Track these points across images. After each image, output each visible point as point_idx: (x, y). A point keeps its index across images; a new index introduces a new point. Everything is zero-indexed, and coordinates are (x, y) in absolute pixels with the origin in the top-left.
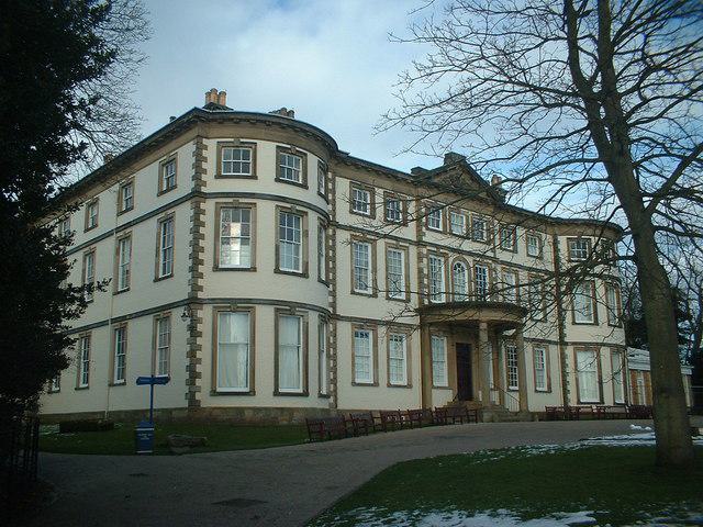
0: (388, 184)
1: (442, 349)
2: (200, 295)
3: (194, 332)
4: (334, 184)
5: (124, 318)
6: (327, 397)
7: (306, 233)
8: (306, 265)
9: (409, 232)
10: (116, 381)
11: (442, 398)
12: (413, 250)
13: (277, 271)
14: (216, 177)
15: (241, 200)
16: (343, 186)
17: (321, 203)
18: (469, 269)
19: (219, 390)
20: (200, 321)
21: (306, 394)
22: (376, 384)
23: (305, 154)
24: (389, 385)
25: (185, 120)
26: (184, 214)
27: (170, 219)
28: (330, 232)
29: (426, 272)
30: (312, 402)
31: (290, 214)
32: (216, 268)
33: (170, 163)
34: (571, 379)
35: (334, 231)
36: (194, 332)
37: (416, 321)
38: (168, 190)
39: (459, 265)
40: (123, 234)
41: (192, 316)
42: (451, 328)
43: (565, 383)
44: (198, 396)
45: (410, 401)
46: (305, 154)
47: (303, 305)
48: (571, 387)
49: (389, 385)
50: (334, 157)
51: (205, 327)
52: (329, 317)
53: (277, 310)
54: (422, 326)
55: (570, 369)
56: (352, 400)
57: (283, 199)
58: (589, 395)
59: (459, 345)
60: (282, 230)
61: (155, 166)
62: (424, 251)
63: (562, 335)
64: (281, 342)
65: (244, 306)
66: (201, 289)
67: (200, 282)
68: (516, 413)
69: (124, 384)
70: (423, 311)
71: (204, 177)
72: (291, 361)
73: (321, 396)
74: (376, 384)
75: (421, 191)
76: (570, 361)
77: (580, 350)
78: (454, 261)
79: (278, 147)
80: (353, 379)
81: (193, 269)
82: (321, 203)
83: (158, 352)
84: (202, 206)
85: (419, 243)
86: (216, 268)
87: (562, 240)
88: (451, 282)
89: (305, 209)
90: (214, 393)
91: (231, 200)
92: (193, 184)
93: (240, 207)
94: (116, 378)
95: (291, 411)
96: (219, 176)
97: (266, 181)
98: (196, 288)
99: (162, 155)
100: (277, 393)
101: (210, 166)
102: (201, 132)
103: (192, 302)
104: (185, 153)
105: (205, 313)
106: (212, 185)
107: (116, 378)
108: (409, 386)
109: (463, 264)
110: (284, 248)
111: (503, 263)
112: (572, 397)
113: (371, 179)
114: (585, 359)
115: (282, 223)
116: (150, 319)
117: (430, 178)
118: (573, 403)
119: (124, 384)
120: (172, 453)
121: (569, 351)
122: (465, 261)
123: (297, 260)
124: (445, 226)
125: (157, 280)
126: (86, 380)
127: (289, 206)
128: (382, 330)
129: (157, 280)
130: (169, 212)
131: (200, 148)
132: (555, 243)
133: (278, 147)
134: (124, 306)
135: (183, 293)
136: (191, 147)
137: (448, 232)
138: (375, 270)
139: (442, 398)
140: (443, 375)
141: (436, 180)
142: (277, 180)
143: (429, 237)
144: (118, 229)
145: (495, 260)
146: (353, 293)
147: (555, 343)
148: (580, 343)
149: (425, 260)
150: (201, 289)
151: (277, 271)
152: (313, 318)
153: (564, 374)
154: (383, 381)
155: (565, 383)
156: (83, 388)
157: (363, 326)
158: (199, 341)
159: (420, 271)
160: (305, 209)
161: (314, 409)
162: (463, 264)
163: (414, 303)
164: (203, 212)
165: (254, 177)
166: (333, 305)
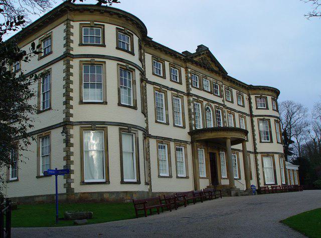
0: (171, 60)
1: (202, 155)
2: (71, 119)
3: (67, 142)
4: (144, 56)
7: (134, 82)
8: (135, 101)
9: (183, 88)
10: (11, 179)
11: (204, 184)
12: (185, 98)
13: (120, 104)
14: (79, 45)
15: (96, 59)
16: (148, 58)
17: (139, 64)
18: (213, 110)
19: (86, 181)
20: (71, 136)
21: (138, 182)
22: (170, 176)
23: (132, 35)
24: (177, 177)
26: (58, 70)
28: (144, 84)
29: (193, 111)
30: (142, 188)
31: (126, 69)
32: (81, 102)
34: (260, 172)
36: (67, 142)
37: (188, 139)
39: (208, 108)
41: (66, 133)
42: (207, 143)
43: (258, 175)
44: (73, 186)
45: (186, 186)
46: (105, 62)
47: (135, 127)
48: (261, 176)
49: (177, 177)
50: (147, 43)
51: (74, 140)
52: (147, 135)
53: (120, 129)
54: (192, 143)
55: (260, 167)
56: (161, 186)
58: (270, 181)
59: (211, 154)
60: (121, 79)
62: (191, 99)
63: (255, 148)
64: (124, 150)
65: (100, 127)
66: (72, 115)
67: (71, 111)
68: (245, 191)
69: (17, 180)
70: (192, 133)
71: (72, 45)
72: (128, 162)
74: (170, 176)
75: (189, 65)
76: (259, 162)
77: (264, 156)
78: (206, 105)
79: (117, 28)
80: (159, 174)
81: (66, 103)
82: (139, 64)
83: (41, 159)
84: (71, 63)
85: (189, 94)
86: (81, 102)
87: (253, 97)
88: (205, 120)
89: (134, 68)
90: (83, 183)
91: (89, 59)
92: (64, 49)
93: (94, 64)
94: (11, 176)
95: (131, 193)
96: (81, 45)
97: (110, 49)
98: (68, 115)
99: (42, 34)
100: (122, 182)
101: (75, 38)
102: (69, 17)
103: (66, 125)
104: (58, 32)
105: (75, 131)
106: (77, 50)
108: (187, 177)
109: (210, 108)
110: (122, 90)
111: (227, 108)
112: (261, 181)
113: (163, 56)
114: (267, 162)
115: (121, 75)
117: (192, 58)
118: (262, 185)
119: (17, 180)
120: (76, 224)
121: (259, 157)
122: (211, 106)
123: (130, 99)
124: (200, 85)
127: (125, 64)
128: (172, 144)
130: (47, 69)
131: (69, 27)
132: (250, 99)
135: (60, 118)
136: (63, 27)
137: (201, 89)
138: (167, 109)
139: (204, 184)
140: (203, 172)
141: (195, 59)
142: (118, 48)
143: (194, 91)
145: (224, 106)
146: (156, 122)
147: (252, 153)
148: (265, 153)
149: (192, 104)
150: (72, 115)
151: (120, 104)
152: (140, 134)
153: (257, 170)
154: (174, 175)
155: (258, 175)
157: (163, 141)
158: (72, 149)
159: (190, 110)
160: (134, 68)
161: (143, 192)
162: (210, 108)
163: (187, 129)
164: (72, 67)
165: (104, 46)
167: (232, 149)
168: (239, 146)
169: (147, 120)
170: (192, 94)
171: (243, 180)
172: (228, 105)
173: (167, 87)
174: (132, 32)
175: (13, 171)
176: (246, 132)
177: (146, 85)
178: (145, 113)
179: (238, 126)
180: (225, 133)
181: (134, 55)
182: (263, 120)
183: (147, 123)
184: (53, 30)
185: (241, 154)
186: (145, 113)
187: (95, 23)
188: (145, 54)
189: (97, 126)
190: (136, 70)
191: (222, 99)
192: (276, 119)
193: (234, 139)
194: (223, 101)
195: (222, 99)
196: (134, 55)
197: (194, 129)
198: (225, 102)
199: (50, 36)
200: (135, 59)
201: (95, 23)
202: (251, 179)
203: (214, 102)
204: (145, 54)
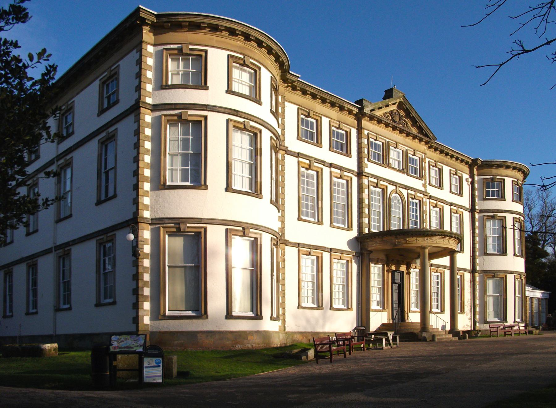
4: (283, 108)
5: (68, 244)
6: (277, 319)
13: (229, 188)
17: (271, 120)
23: (260, 69)
25: (128, 25)
27: (112, 138)
33: (114, 76)
35: (283, 156)
38: (110, 106)
40: (64, 162)
57: (236, 113)
61: (97, 83)
73: (272, 318)
79: (229, 56)
82: (271, 120)
94: (62, 302)
107: (62, 302)
111: (430, 197)
116: (92, 245)
125: (99, 202)
126: (35, 306)
127: (241, 120)
128: (326, 256)
129: (99, 202)
133: (231, 56)
134: (67, 232)
144: (59, 157)
145: (425, 193)
146: (299, 219)
152: (266, 241)
156: (33, 314)
166: (283, 229)
167: (431, 265)
168: (445, 261)
169: (283, 216)
170: (368, 174)
171: (446, 316)
172: (433, 191)
173: (324, 162)
174: (260, 63)
175: (65, 295)
176: (459, 239)
177: (283, 156)
178: (277, 202)
179: (447, 228)
180: (441, 240)
181: (260, 104)
182: (180, 120)
183: (283, 222)
184: (119, 63)
185: (447, 273)
186: (277, 202)
187: (191, 47)
188: (286, 103)
189: (188, 225)
190: (264, 130)
191: (423, 182)
192: (517, 216)
193: (440, 249)
194: (424, 186)
195: (423, 182)
196: (260, 104)
197: (366, 231)
198: (429, 187)
199: (116, 73)
200: (263, 111)
201: (191, 47)
202: (462, 311)
203: (406, 188)
204: (286, 103)
